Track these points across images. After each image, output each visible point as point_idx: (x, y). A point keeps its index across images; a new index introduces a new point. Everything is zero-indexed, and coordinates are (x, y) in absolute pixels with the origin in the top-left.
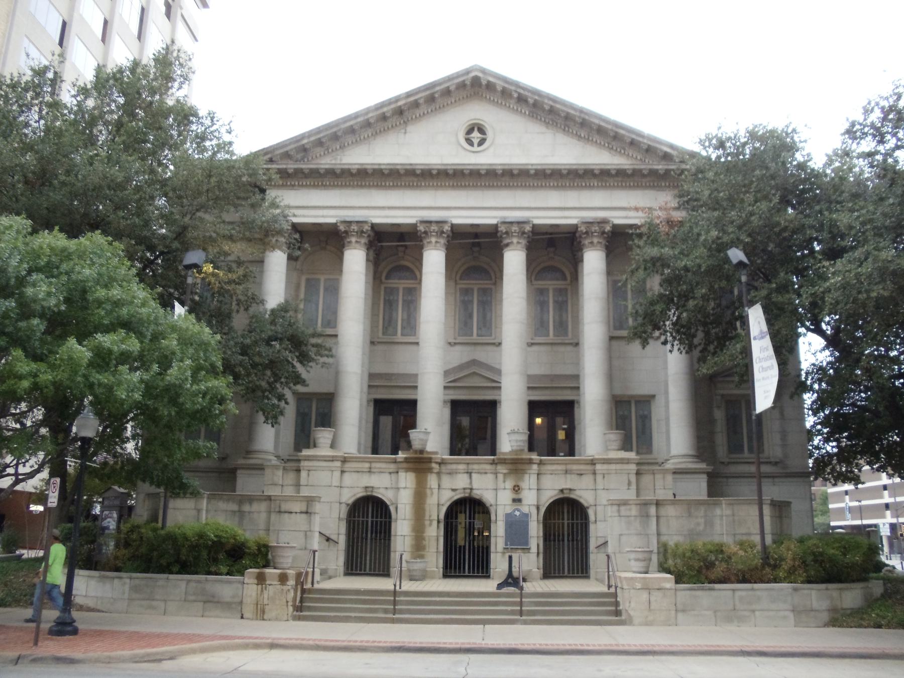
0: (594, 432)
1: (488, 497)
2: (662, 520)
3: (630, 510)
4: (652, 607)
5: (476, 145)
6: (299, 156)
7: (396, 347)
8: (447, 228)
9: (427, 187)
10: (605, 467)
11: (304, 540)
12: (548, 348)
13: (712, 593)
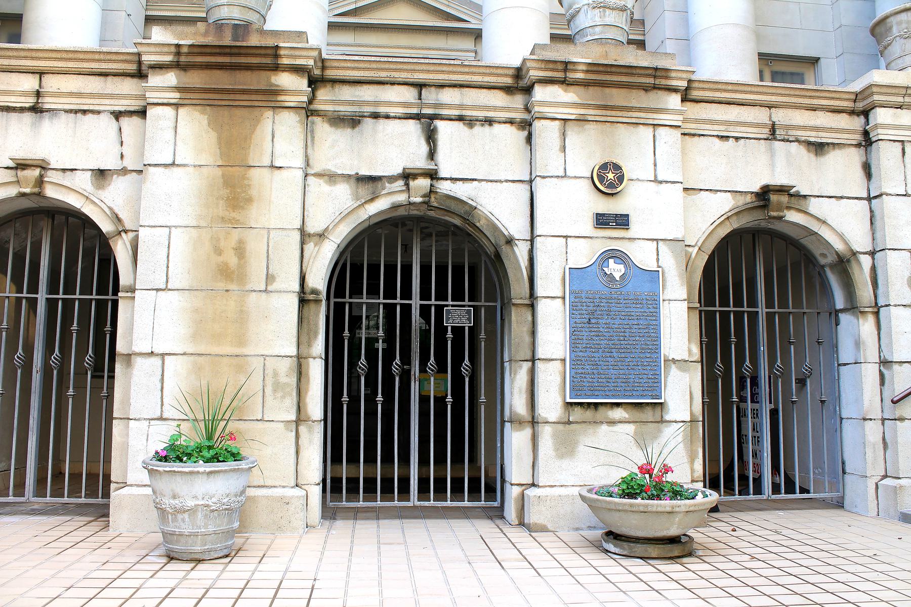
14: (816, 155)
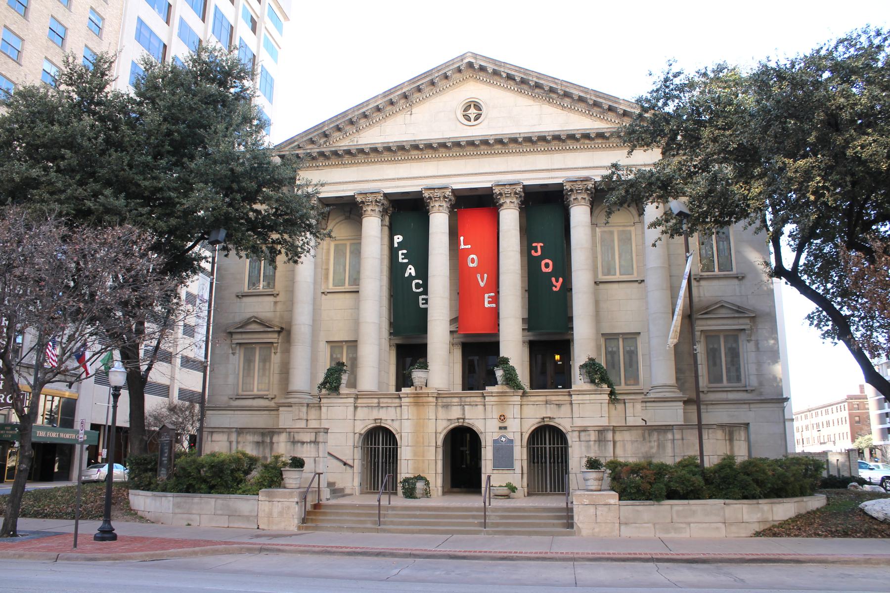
1: (478, 426)
3: (589, 435)
4: (598, 520)
5: (472, 119)
6: (322, 141)
10: (580, 397)
11: (313, 465)
14: (269, 125)
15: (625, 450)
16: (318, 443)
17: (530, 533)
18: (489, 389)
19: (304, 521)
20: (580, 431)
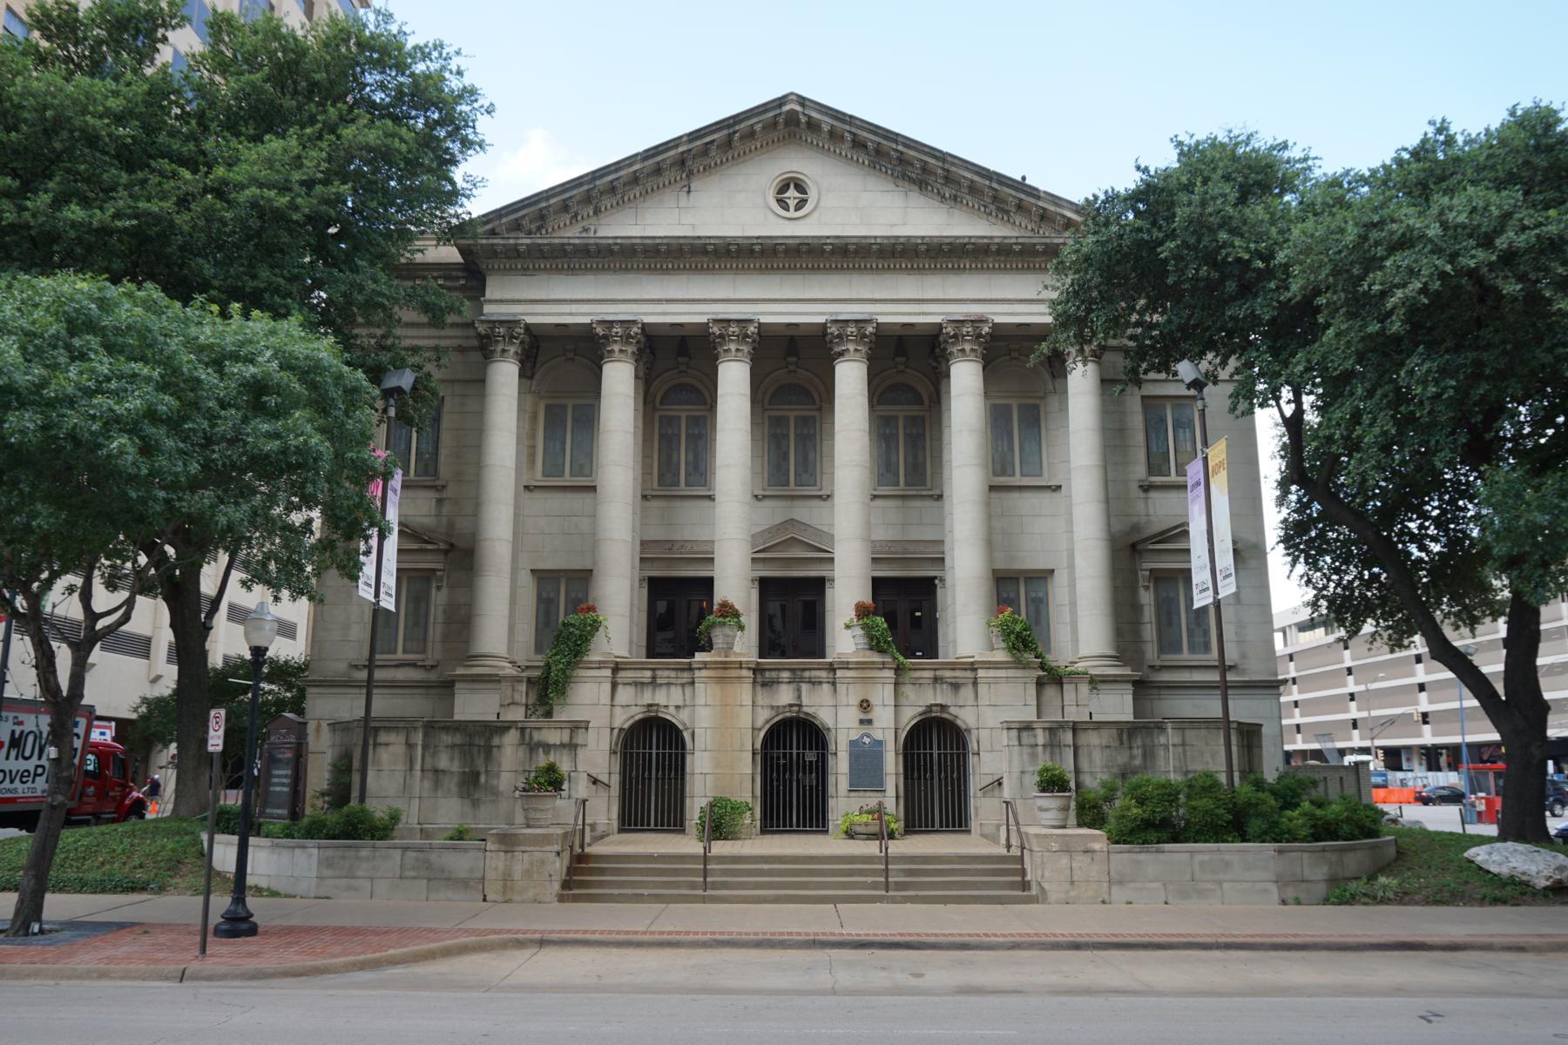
0: (966, 625)
1: (825, 716)
2: (1083, 753)
7: (678, 503)
8: (752, 329)
9: (723, 270)
10: (992, 673)
12: (898, 503)
13: (1161, 856)
15: (1091, 761)
16: (576, 746)
17: (945, 900)
18: (700, 657)
19: (566, 885)
20: (1020, 730)
